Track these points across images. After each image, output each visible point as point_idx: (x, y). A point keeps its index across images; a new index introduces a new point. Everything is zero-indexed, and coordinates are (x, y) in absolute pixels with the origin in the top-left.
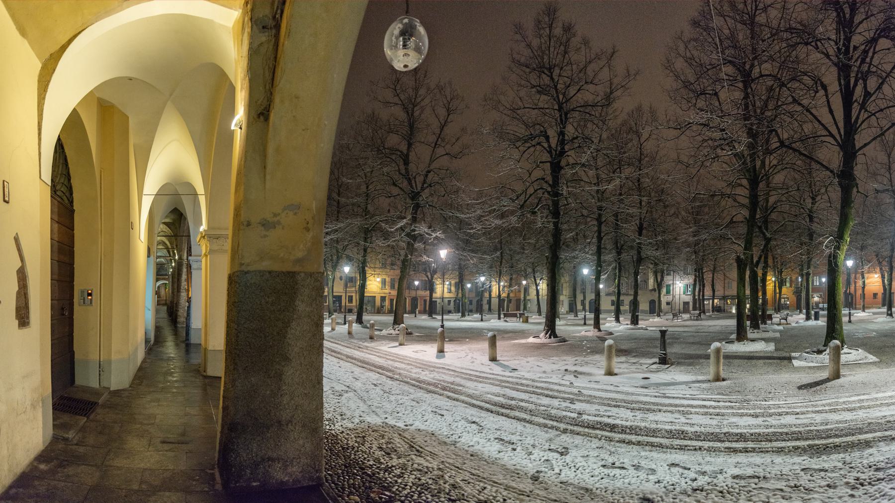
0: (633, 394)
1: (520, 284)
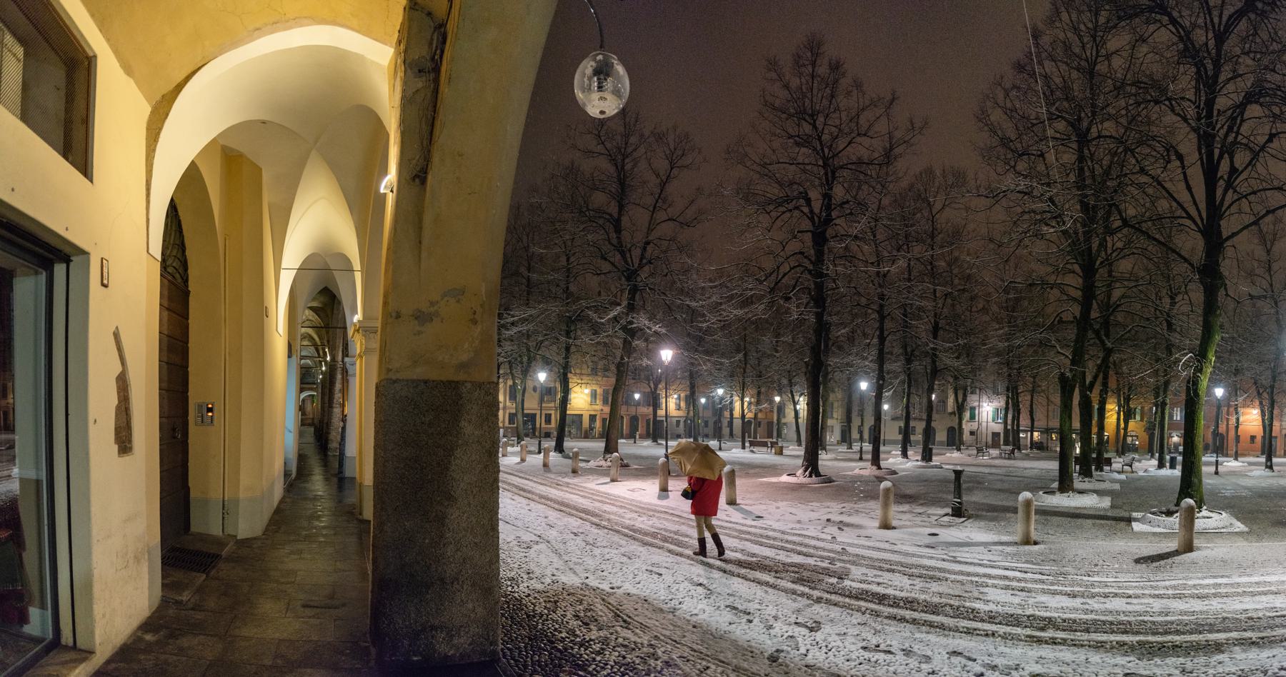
0: (913, 555)
1: (772, 402)
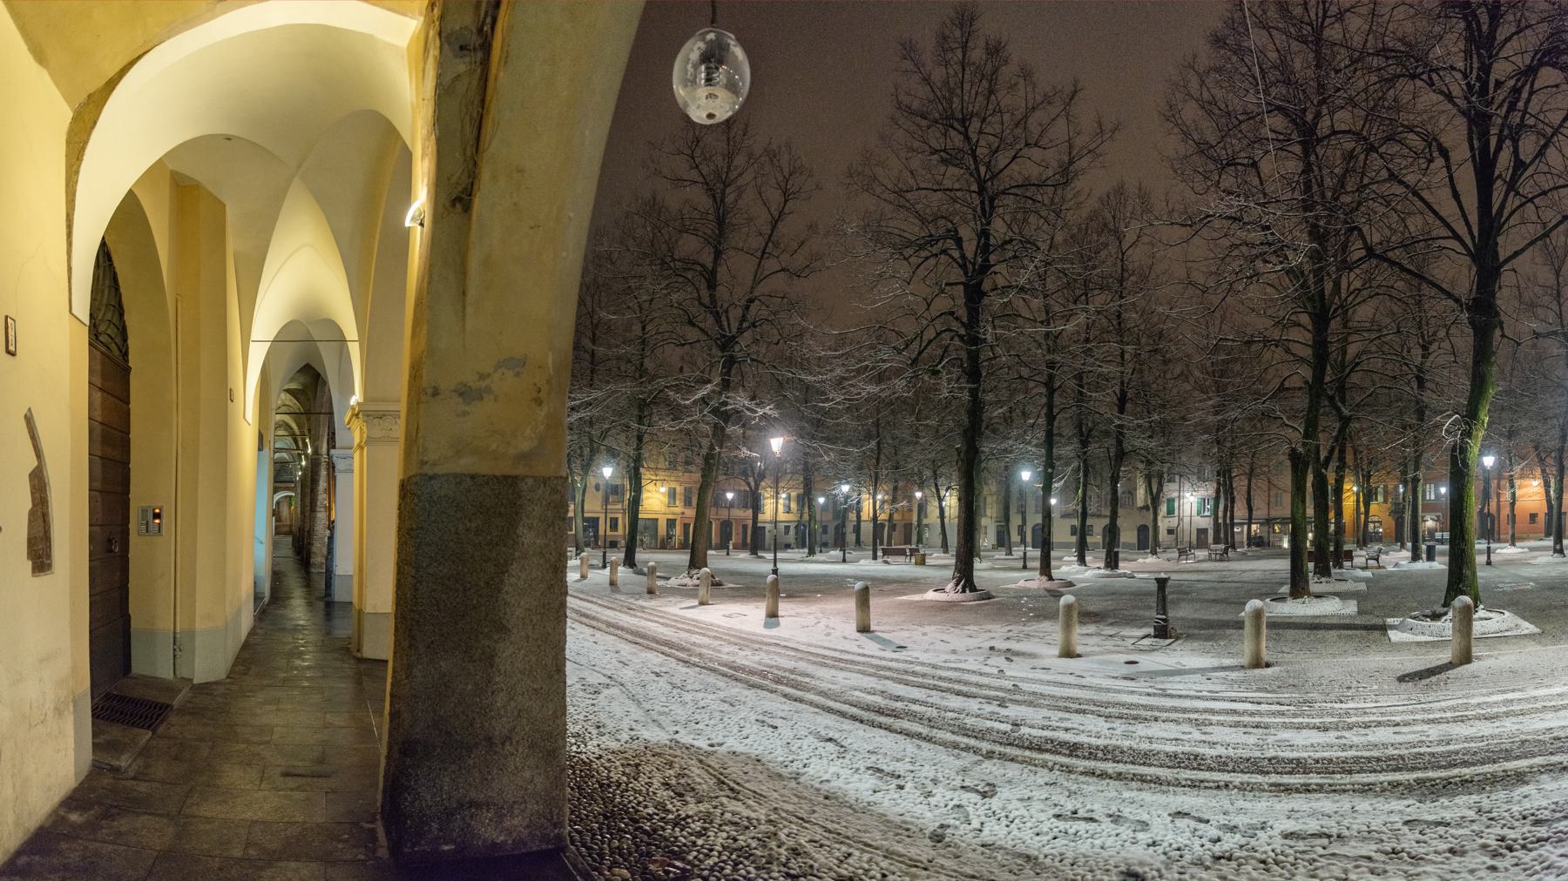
0: (1108, 690)
1: (910, 498)
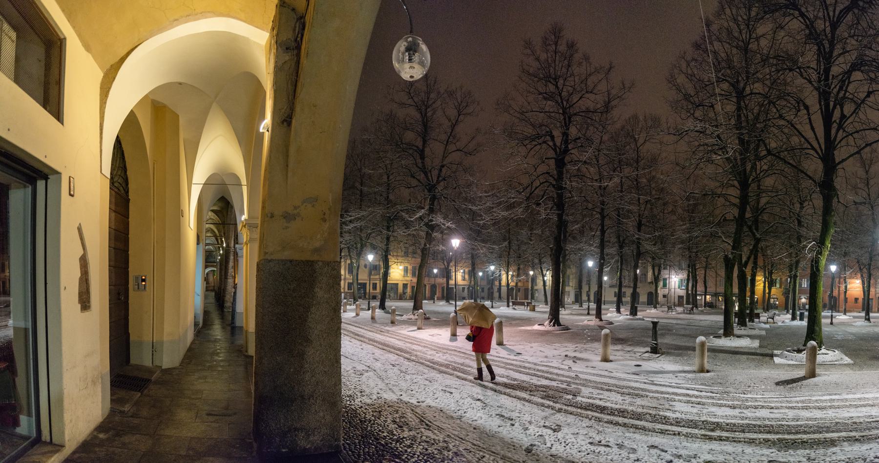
0: (624, 380)
1: (527, 275)
